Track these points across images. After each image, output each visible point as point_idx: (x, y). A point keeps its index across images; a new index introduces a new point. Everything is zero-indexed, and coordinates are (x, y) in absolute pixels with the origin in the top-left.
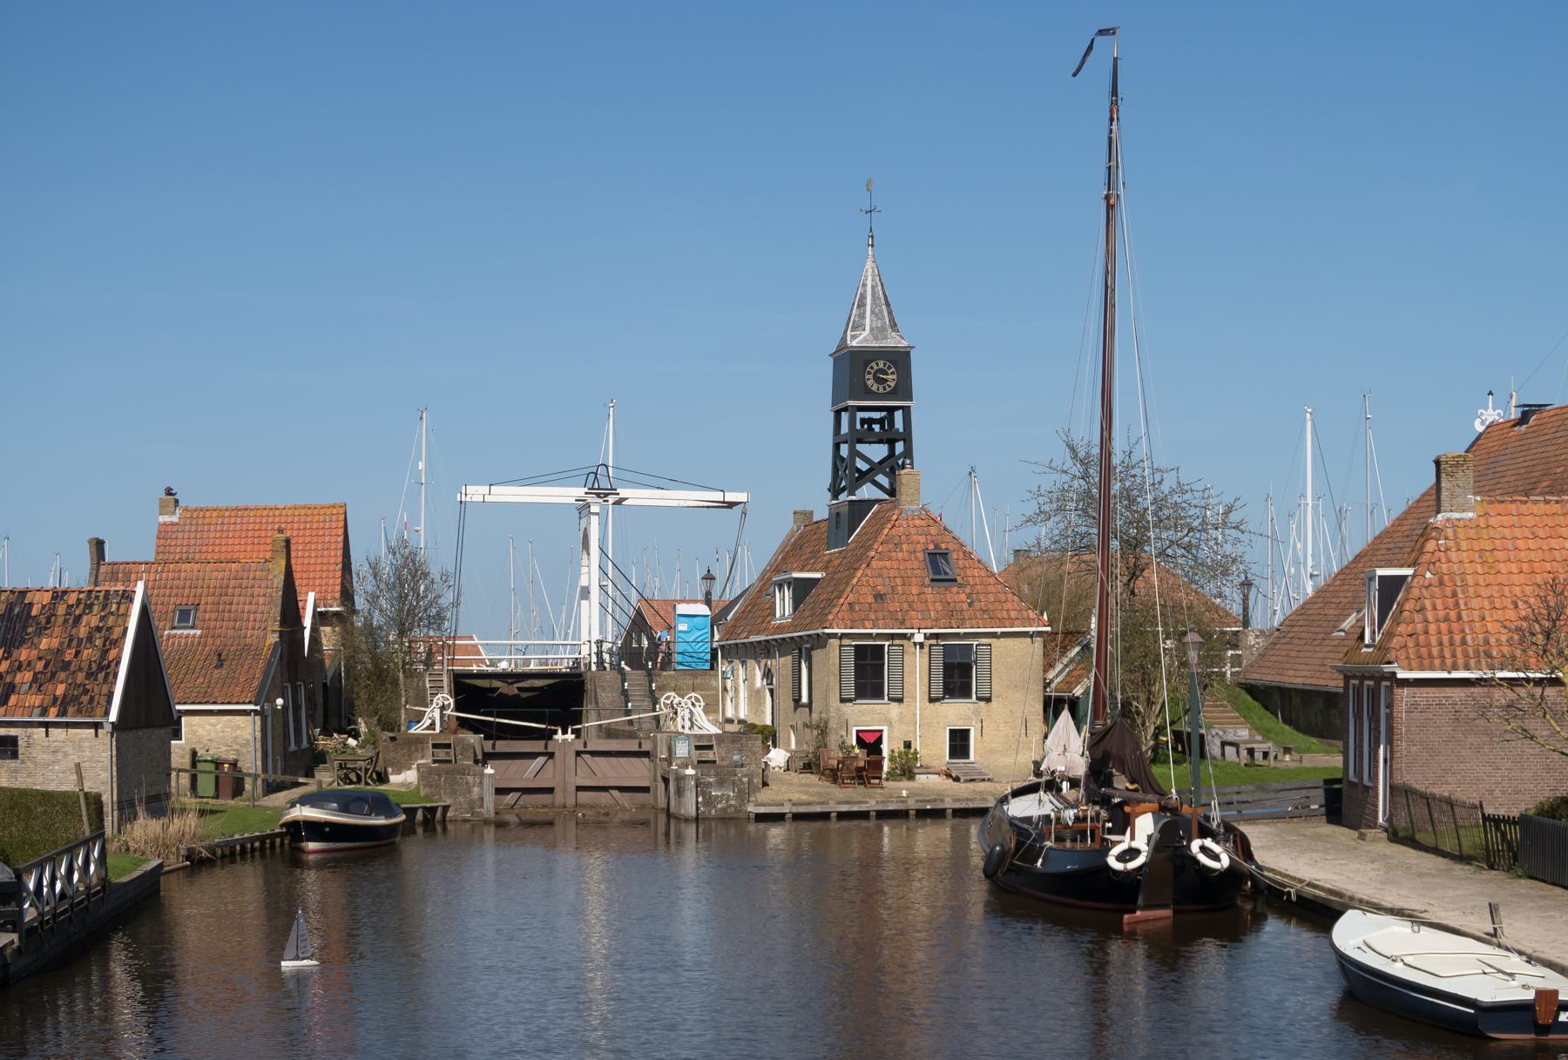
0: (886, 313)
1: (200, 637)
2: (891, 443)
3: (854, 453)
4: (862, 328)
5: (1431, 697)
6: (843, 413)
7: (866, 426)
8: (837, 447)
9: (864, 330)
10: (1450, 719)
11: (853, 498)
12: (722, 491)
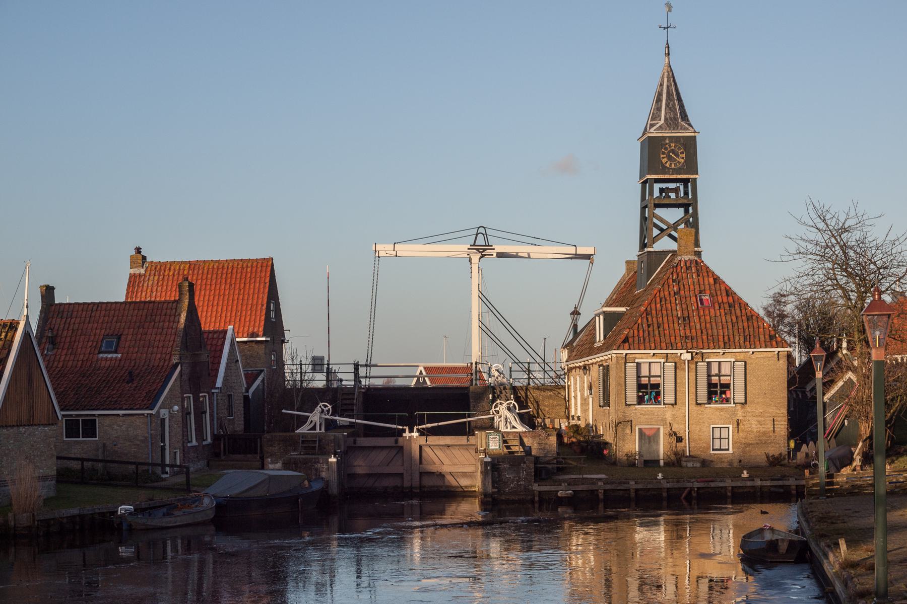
0: (677, 107)
1: (120, 360)
4: (659, 119)
7: (664, 194)
8: (643, 208)
9: (660, 120)
12: (575, 246)
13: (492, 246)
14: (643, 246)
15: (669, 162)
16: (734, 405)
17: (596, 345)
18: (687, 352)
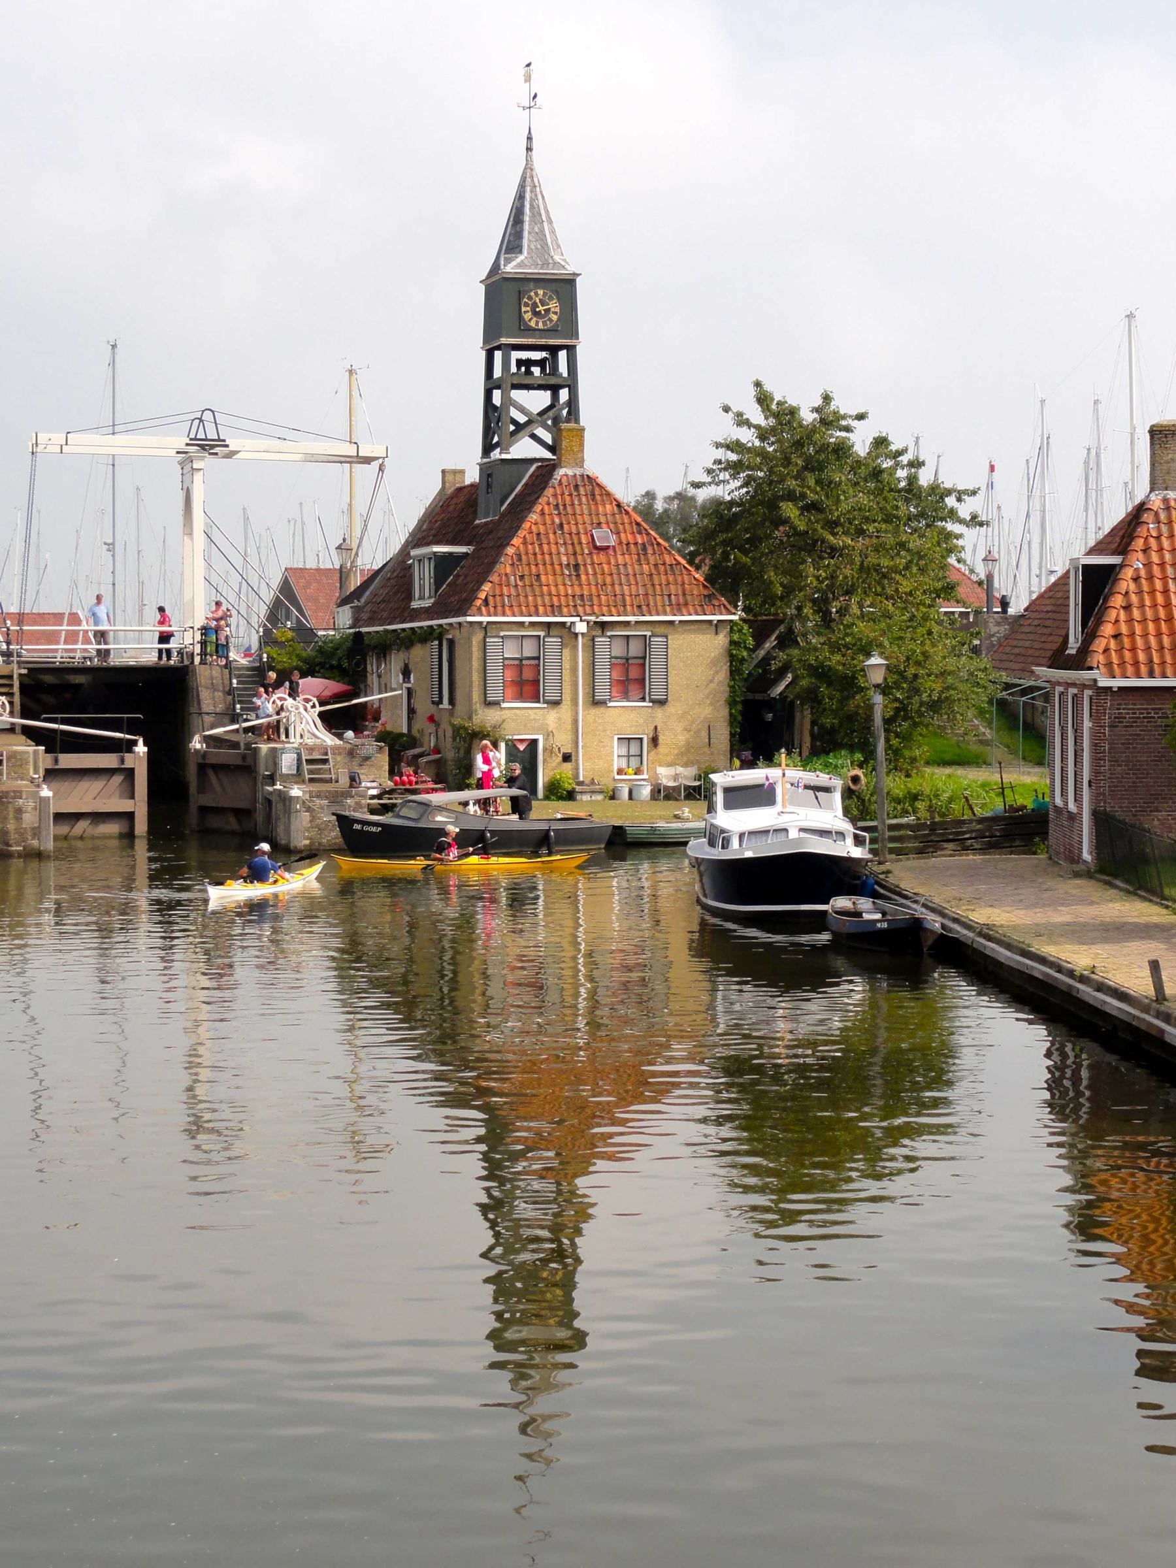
2: (555, 389)
3: (508, 401)
4: (518, 250)
5: (1138, 709)
6: (496, 352)
7: (523, 369)
10: (1159, 735)
11: (504, 456)
13: (224, 441)
14: (488, 448)
15: (535, 319)
16: (651, 704)
17: (415, 604)
18: (581, 620)
